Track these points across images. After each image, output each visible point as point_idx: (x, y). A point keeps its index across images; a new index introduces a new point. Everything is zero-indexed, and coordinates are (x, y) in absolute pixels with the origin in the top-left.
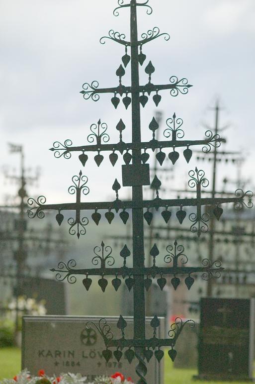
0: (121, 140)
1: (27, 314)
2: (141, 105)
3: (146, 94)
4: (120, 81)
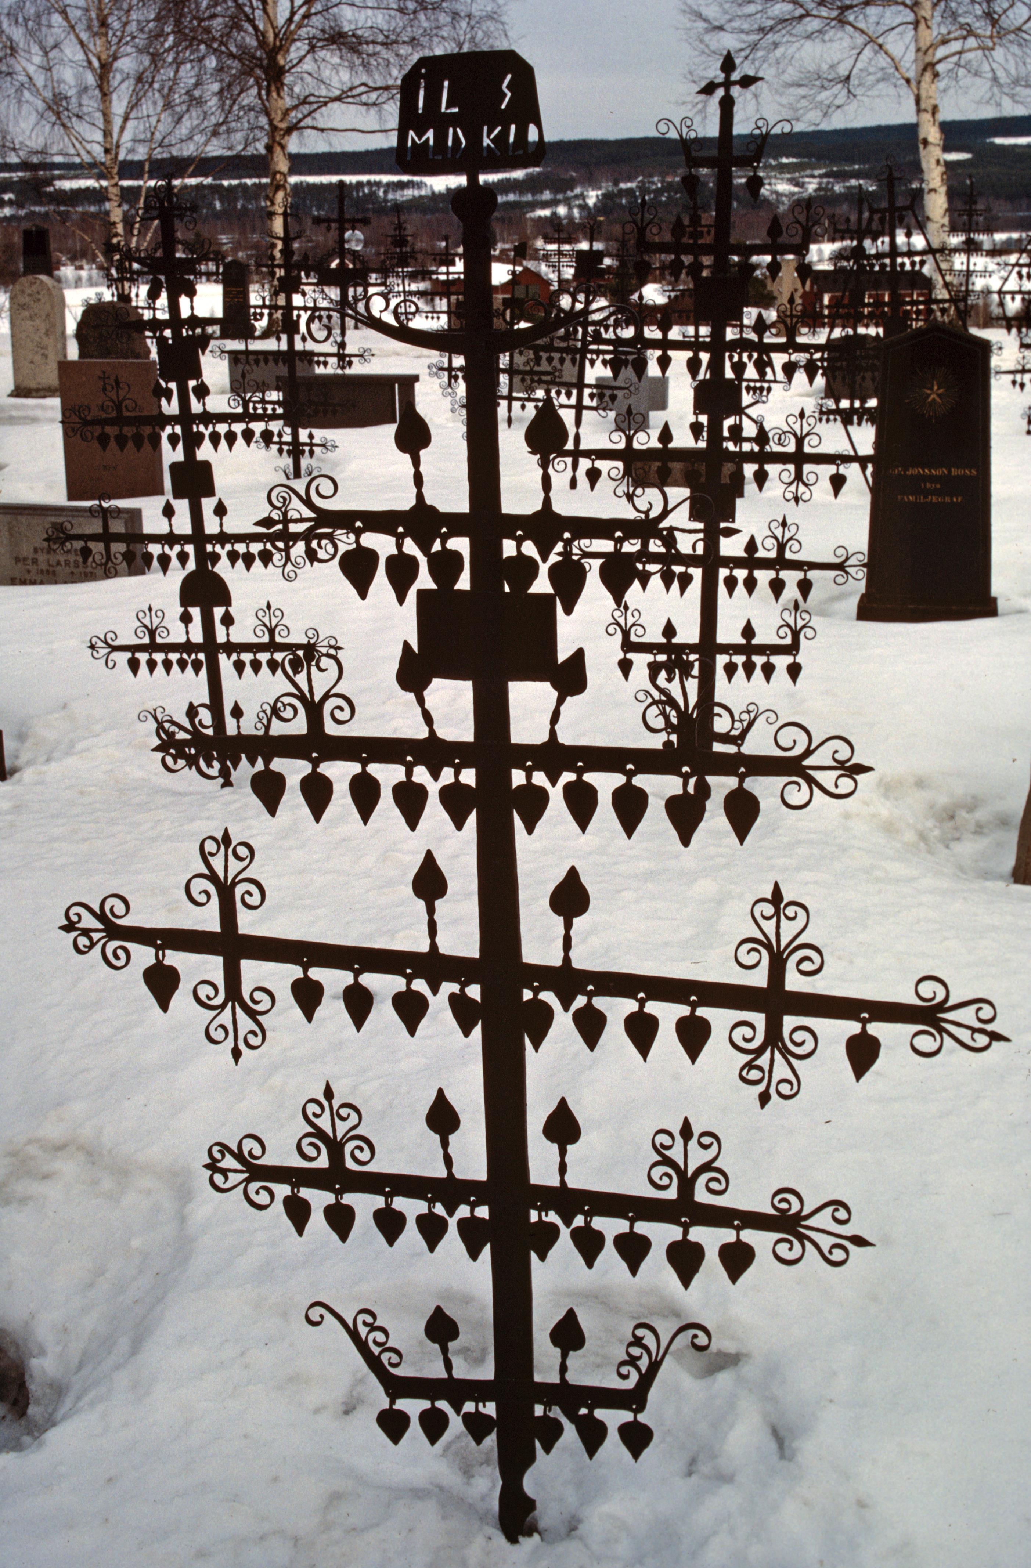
0: (420, 496)
1: (54, 525)
2: (518, 823)
3: (540, 778)
4: (221, 525)
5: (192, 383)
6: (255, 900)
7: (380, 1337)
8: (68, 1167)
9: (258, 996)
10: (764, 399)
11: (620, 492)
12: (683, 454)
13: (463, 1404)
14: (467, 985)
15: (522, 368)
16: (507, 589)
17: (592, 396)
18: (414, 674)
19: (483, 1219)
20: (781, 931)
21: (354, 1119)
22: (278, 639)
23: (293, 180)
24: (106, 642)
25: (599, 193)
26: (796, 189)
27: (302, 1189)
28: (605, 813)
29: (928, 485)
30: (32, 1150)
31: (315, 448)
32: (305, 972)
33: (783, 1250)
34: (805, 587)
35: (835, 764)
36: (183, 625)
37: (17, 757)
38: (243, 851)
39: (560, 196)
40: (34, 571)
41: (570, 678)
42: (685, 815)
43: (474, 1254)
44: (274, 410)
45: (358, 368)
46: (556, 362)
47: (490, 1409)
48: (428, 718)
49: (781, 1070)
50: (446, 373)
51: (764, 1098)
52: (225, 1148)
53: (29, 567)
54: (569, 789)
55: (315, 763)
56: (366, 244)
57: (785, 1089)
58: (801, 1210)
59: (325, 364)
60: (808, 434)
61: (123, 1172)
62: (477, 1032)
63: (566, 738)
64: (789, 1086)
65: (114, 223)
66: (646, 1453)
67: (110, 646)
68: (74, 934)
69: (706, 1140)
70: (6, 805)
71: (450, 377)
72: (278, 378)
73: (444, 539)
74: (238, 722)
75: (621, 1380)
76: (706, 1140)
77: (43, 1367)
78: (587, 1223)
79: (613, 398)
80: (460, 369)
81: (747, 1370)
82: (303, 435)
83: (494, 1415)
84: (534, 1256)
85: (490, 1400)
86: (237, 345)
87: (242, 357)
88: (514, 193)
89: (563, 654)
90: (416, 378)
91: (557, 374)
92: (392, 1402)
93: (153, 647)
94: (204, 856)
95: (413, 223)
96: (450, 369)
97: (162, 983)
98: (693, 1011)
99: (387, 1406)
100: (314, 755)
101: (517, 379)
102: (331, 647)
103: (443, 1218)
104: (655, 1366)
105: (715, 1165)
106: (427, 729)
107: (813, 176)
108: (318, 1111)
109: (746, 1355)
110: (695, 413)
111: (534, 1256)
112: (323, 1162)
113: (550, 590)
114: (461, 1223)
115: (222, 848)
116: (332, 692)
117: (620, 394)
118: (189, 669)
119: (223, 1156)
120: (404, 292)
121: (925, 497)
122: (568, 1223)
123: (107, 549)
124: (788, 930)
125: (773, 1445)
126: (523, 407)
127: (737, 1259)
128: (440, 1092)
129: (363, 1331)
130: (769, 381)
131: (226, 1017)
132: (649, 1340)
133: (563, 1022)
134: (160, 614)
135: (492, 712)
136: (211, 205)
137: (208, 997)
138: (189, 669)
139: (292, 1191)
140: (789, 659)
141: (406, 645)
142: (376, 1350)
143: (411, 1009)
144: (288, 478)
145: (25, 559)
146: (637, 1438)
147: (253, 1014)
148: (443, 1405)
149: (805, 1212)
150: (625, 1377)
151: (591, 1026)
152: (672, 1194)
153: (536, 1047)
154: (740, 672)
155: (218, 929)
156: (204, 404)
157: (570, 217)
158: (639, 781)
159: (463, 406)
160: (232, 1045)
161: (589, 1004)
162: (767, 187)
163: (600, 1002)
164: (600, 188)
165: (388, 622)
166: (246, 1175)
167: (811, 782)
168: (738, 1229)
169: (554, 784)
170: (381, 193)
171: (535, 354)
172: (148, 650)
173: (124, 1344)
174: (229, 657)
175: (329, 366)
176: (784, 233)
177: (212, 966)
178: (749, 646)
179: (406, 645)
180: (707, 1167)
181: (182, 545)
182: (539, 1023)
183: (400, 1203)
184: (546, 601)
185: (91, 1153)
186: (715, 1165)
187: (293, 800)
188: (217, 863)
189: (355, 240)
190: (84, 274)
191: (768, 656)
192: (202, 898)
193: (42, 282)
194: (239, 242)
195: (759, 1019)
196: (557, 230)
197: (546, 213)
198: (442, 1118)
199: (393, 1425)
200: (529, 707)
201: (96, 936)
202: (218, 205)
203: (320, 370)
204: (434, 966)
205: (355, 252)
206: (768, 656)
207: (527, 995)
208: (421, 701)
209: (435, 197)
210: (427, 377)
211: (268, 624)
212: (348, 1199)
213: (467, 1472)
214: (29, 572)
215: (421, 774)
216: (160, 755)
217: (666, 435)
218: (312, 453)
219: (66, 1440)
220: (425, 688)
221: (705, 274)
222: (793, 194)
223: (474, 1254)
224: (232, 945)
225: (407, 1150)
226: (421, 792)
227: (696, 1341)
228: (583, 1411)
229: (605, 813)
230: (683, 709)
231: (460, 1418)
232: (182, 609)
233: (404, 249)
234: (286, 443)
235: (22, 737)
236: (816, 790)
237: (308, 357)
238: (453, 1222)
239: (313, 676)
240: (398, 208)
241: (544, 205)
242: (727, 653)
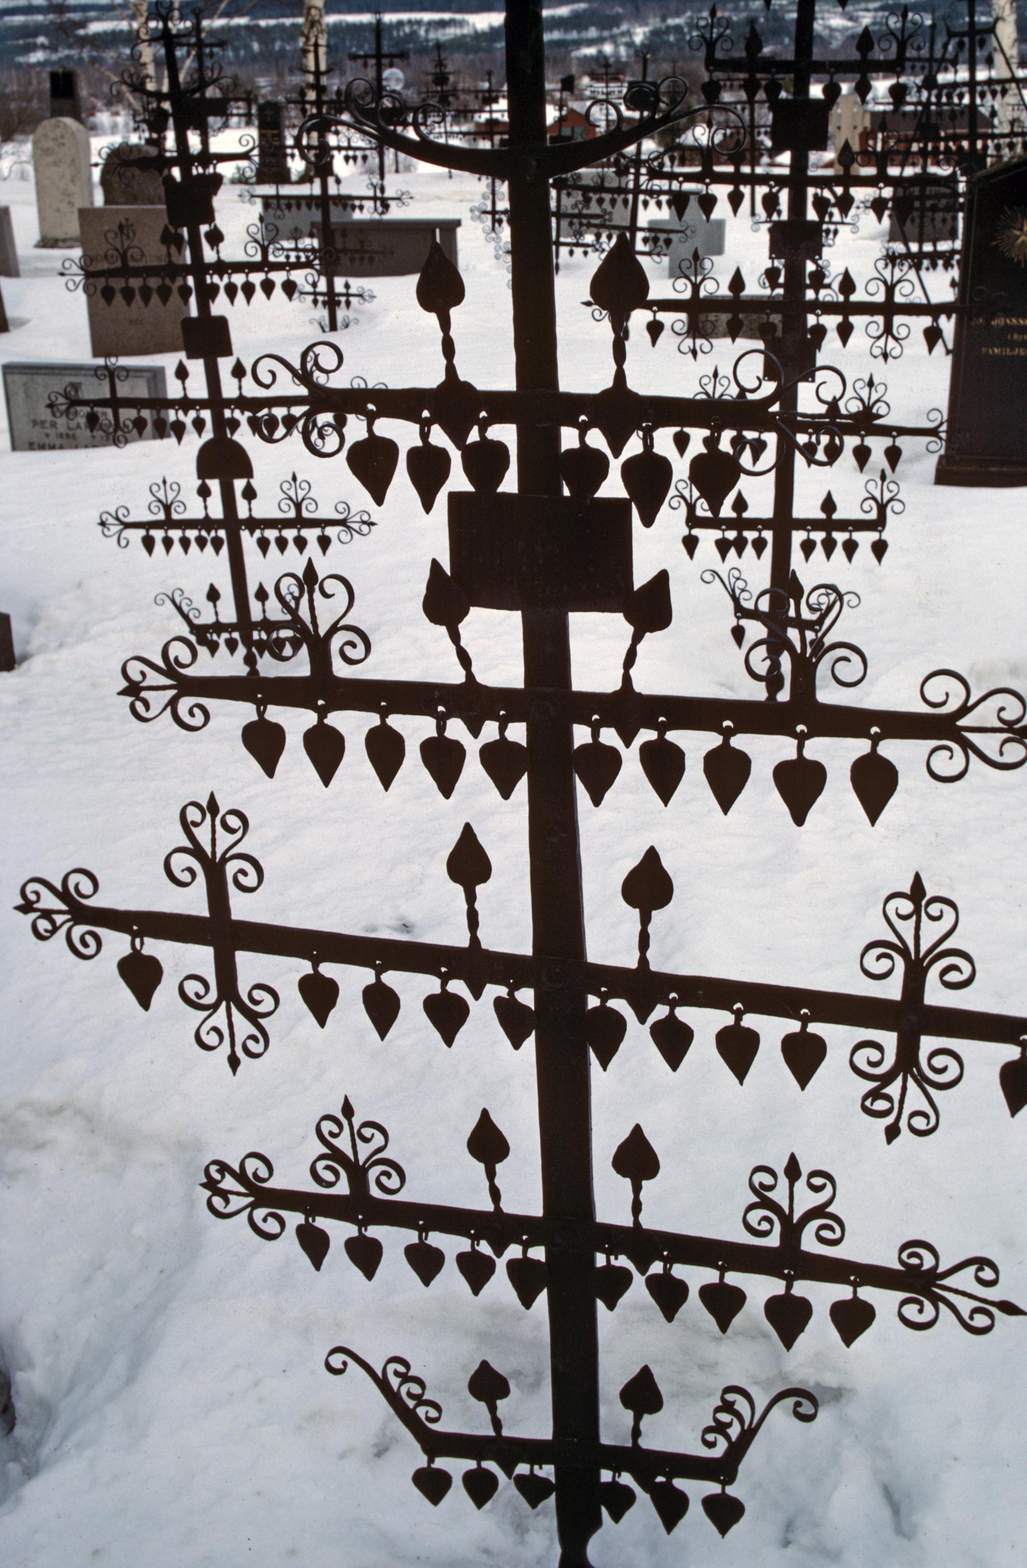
0: (451, 370)
3: (609, 737)
4: (240, 388)
5: (204, 228)
6: (250, 880)
7: (416, 1389)
8: (64, 1135)
9: (258, 994)
10: (830, 242)
11: (684, 348)
12: (757, 304)
13: (516, 1465)
14: (518, 989)
15: (570, 211)
16: (566, 492)
17: (645, 240)
18: (446, 601)
19: (539, 1261)
20: (921, 933)
21: (379, 1140)
22: (305, 514)
23: (331, 19)
24: (117, 519)
25: (647, 29)
26: (850, 24)
27: (318, 1219)
28: (694, 779)
29: (1015, 337)
30: (24, 1115)
31: (352, 299)
32: (315, 967)
33: (911, 1311)
34: (893, 455)
35: (999, 725)
36: (200, 499)
37: (28, 642)
38: (234, 822)
39: (606, 34)
40: (53, 436)
41: (650, 609)
42: (800, 786)
43: (527, 1301)
44: (298, 257)
45: (396, 213)
46: (607, 205)
47: (547, 1471)
48: (464, 659)
49: (915, 1099)
50: (489, 217)
51: (892, 1133)
52: (224, 1168)
53: (49, 431)
54: (647, 750)
55: (322, 713)
56: (407, 86)
57: (920, 1123)
58: (937, 1266)
59: (361, 208)
60: (899, 281)
61: (125, 1142)
62: (530, 1043)
63: (645, 682)
64: (925, 1121)
65: (144, 65)
66: (735, 1529)
67: (122, 523)
68: (33, 916)
69: (817, 1181)
70: (9, 700)
71: (494, 221)
72: (313, 225)
73: (484, 426)
74: (263, 605)
75: (706, 1449)
76: (817, 1181)
77: (30, 1383)
78: (667, 1271)
79: (668, 242)
80: (505, 212)
81: (854, 1410)
82: (339, 283)
83: (553, 1479)
84: (600, 1305)
85: (548, 1462)
86: (269, 190)
87: (274, 202)
88: (559, 30)
89: (641, 576)
90: (458, 223)
91: (607, 217)
92: (431, 1461)
93: (169, 523)
94: (187, 826)
95: (454, 62)
96: (493, 212)
97: (141, 976)
98: (804, 1026)
99: (425, 1465)
100: (321, 702)
101: (564, 223)
102: (364, 522)
103: (489, 1258)
104: (748, 1435)
105: (830, 1209)
106: (463, 673)
107: (867, 10)
108: (336, 1130)
109: (850, 1391)
110: (771, 258)
111: (600, 1305)
112: (342, 1188)
113: (623, 494)
114: (512, 1265)
115: (208, 816)
116: (341, 624)
117: (674, 237)
118: (209, 548)
119: (223, 1177)
120: (446, 133)
121: (1012, 349)
122: (643, 1270)
123: (116, 415)
124: (931, 932)
125: (886, 1513)
126: (571, 253)
127: (852, 1320)
128: (485, 1113)
129: (395, 1382)
130: (836, 223)
131: (219, 1019)
132: (742, 1406)
133: (638, 1037)
134: (175, 487)
135: (547, 652)
136: (248, 47)
137: (197, 995)
138: (209, 548)
139: (307, 1220)
140: (873, 536)
141: (435, 564)
142: (411, 1403)
143: (447, 1016)
144: (324, 331)
145: (43, 422)
146: (725, 1513)
147: (253, 1017)
148: (490, 1465)
149: (941, 1269)
150: (711, 1445)
151: (673, 1042)
152: (773, 1241)
153: (604, 1065)
154: (819, 551)
155: (206, 913)
156: (218, 252)
157: (616, 55)
158: (739, 742)
159: (508, 252)
160: (229, 1052)
161: (672, 1016)
162: (820, 22)
163: (685, 1014)
164: (647, 25)
165: (413, 534)
166: (251, 1199)
167: (967, 746)
168: (855, 1285)
169: (628, 744)
170: (422, 32)
171: (584, 195)
172: (164, 527)
173: (120, 1364)
174: (252, 533)
175: (365, 210)
176: (876, 46)
177: (200, 958)
178: (829, 521)
179: (435, 565)
180: (819, 1212)
181: (198, 411)
182: (608, 1036)
183: (436, 1239)
184: (619, 508)
185: (90, 1120)
186: (830, 1209)
187: (295, 757)
188: (203, 834)
189: (394, 78)
190: (120, 120)
191: (851, 532)
192: (186, 877)
193: (65, 125)
194: (277, 86)
195: (889, 1039)
196: (604, 69)
197: (591, 51)
198: (488, 1144)
199: (432, 1485)
200: (597, 649)
201: (59, 919)
202: (256, 46)
203: (357, 215)
204: (475, 964)
205: (394, 91)
206: (851, 532)
207: (593, 1002)
208: (455, 637)
209: (478, 36)
210: (470, 222)
211: (294, 497)
212: (374, 1231)
213: (521, 1528)
214: (47, 435)
215: (456, 729)
216: (130, 699)
217: (737, 282)
218: (348, 304)
219: (49, 1496)
220: (461, 620)
221: (783, 95)
222: (846, 29)
223: (527, 1301)
224: (224, 934)
225: (445, 1176)
226: (457, 752)
227: (799, 1409)
228: (660, 1479)
229: (694, 779)
230: (799, 651)
231: (512, 1481)
232: (200, 482)
233: (445, 88)
234: (321, 294)
235: (33, 620)
236: (973, 757)
237: (346, 202)
238: (501, 1264)
239: (316, 604)
240: (439, 46)
241: (590, 43)
242: (804, 529)
